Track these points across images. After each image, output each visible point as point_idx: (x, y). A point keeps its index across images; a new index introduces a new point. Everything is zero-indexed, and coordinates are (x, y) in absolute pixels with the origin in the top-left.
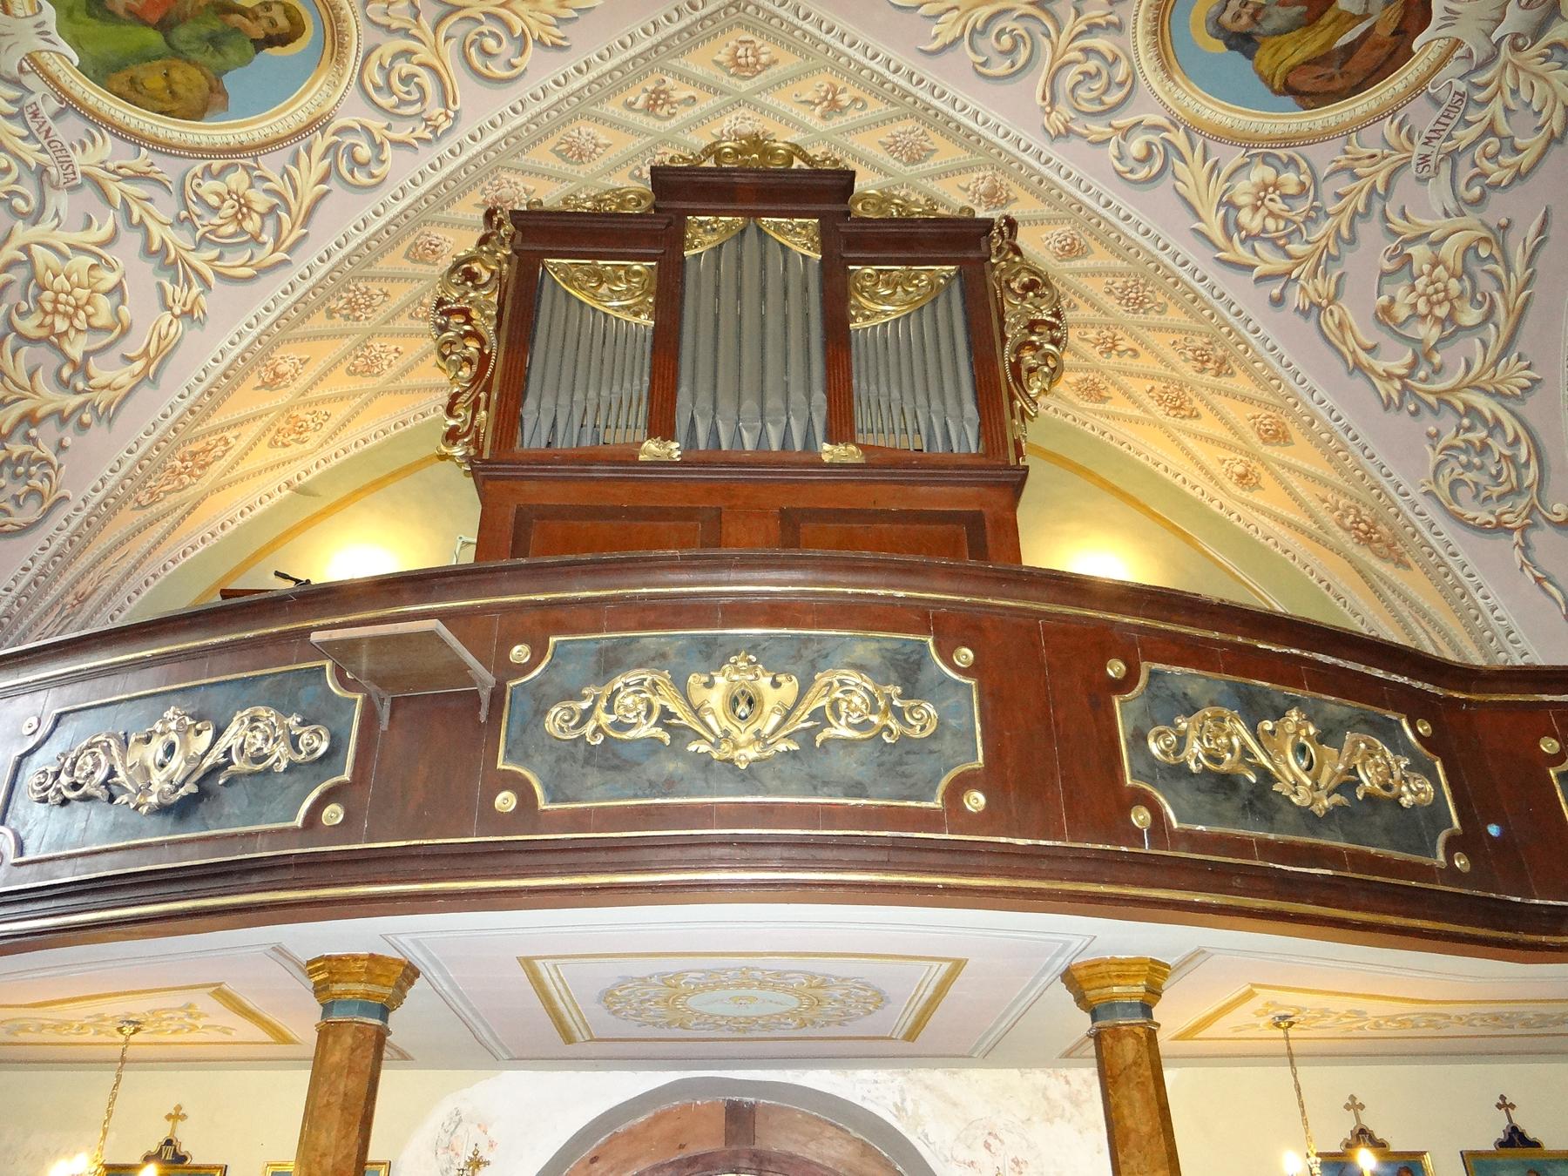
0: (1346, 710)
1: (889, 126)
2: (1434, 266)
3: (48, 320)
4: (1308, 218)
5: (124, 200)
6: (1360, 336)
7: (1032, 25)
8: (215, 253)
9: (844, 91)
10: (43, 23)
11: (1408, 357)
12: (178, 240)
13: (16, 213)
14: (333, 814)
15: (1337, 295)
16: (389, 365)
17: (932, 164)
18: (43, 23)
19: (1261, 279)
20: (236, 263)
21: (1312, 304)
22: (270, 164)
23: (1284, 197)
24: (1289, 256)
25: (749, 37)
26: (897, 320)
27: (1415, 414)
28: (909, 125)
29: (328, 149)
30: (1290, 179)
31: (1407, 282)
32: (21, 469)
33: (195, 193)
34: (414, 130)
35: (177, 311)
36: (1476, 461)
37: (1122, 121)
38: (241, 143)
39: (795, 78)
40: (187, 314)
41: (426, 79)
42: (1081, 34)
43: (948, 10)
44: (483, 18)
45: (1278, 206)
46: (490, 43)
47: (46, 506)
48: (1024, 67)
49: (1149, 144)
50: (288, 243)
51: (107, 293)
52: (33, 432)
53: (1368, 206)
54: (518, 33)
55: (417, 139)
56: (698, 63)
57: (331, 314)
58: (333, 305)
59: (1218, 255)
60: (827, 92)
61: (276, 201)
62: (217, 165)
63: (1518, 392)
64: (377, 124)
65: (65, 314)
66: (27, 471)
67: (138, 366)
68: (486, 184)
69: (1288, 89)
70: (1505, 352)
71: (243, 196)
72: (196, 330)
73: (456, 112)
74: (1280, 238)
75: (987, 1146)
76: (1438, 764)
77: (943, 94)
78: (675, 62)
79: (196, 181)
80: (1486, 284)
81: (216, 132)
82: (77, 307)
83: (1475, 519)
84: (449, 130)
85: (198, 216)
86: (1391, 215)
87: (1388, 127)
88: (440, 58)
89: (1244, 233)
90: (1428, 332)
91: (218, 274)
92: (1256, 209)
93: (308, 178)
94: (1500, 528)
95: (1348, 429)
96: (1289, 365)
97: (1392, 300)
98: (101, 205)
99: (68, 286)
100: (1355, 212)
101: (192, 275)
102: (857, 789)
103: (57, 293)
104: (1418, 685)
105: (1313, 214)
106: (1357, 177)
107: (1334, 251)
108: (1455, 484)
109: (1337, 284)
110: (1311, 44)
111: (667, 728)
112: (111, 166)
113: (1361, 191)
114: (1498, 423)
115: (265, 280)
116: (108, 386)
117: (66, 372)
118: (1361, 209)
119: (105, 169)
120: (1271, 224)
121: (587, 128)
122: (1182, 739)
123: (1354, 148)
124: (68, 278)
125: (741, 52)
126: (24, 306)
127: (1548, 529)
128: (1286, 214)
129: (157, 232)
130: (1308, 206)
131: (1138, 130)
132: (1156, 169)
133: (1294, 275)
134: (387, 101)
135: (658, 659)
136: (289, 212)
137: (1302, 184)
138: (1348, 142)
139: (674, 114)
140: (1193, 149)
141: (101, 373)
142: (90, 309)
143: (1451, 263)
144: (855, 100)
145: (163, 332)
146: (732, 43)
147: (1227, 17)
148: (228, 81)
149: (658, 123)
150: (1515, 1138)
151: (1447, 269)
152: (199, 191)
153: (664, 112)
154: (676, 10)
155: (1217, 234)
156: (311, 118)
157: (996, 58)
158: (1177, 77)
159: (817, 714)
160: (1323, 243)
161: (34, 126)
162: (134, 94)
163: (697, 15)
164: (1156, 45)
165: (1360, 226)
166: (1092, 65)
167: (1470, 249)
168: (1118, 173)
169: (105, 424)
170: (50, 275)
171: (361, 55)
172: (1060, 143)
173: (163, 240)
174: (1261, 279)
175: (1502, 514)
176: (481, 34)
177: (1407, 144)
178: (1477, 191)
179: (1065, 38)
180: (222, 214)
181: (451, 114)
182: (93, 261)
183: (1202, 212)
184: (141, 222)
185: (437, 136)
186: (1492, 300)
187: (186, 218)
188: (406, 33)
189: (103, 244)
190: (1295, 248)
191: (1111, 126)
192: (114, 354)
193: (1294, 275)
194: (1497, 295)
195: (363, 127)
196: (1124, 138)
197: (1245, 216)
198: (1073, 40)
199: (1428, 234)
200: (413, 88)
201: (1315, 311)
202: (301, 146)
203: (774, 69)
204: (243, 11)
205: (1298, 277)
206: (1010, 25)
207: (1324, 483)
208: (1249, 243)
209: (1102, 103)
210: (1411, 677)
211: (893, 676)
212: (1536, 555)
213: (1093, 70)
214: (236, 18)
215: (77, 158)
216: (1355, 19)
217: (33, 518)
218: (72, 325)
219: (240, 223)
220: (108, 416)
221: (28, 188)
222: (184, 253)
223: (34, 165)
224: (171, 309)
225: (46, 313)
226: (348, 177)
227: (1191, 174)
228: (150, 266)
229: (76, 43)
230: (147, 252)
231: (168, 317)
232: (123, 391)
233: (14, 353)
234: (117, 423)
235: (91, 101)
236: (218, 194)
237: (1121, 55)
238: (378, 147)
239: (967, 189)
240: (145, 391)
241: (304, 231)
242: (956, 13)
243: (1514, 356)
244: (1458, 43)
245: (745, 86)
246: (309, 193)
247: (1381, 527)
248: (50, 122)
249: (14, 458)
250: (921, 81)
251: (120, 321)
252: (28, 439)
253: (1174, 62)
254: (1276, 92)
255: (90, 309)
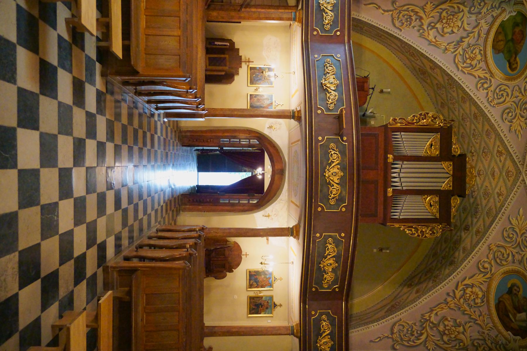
0: (339, 275)
1: (494, 208)
2: (458, 332)
3: (446, 18)
4: (469, 304)
5: (474, 32)
6: (440, 312)
7: (514, 242)
8: (461, 53)
9: (502, 197)
10: (512, 12)
11: (435, 322)
12: (465, 45)
13: (470, 8)
14: (319, 112)
15: (450, 308)
16: (440, 92)
17: (486, 218)
18: (512, 12)
19: (454, 291)
20: (459, 58)
21: (448, 302)
22: (482, 64)
23: (474, 299)
24: (460, 299)
25: (514, 174)
26: (424, 205)
27: (420, 321)
28: (495, 213)
29: (486, 77)
30: (479, 301)
31: (454, 325)
32: (409, 20)
33: (476, 48)
34: (491, 97)
35: (447, 47)
36: (409, 332)
37: (493, 262)
38: (487, 58)
39: (506, 185)
40: (446, 49)
41: (502, 99)
42: (512, 253)
43: (518, 222)
44: (516, 113)
45: (472, 298)
46: (510, 114)
47: (400, 27)
48: (505, 239)
49: (487, 268)
50: (464, 70)
51: (452, 30)
52: (418, 20)
53: (473, 319)
54: (513, 121)
55: (489, 98)
56: (508, 163)
57: (448, 80)
58: (450, 80)
59: (460, 282)
60: (502, 193)
61: (474, 66)
62: (482, 52)
63: (427, 345)
64: (492, 88)
65: (447, 21)
66: (408, 21)
67: (434, 40)
68: (479, 114)
69: (500, 302)
70: (436, 344)
71: (475, 59)
72: (442, 52)
73: (495, 107)
74: (464, 297)
75: (275, 214)
76: (330, 290)
77: (500, 220)
78: (508, 157)
79: (479, 48)
80: (454, 344)
81: (490, 52)
82: (449, 24)
83: (395, 328)
84: (491, 105)
85: (470, 49)
86: (470, 323)
87: (491, 325)
88: (507, 103)
89: (465, 289)
90: (441, 328)
91: (456, 55)
92: (472, 292)
93: (481, 73)
94: (392, 333)
95: (417, 305)
96: (432, 295)
97: (449, 321)
98: (473, 26)
99: (454, 21)
100: (471, 315)
101: (455, 49)
102: (321, 191)
103: (452, 19)
104: (345, 290)
105: (470, 305)
106: (479, 316)
107: (461, 309)
108: (404, 327)
109: (453, 309)
110: (510, 308)
111: (331, 162)
112: (482, 29)
113: (476, 317)
114: (419, 339)
115: (454, 65)
116: (429, 34)
117: (433, 24)
118: (472, 317)
119: (481, 27)
120: (468, 295)
121: (493, 136)
122: (331, 244)
123: (486, 317)
124: (456, 21)
125: (511, 173)
126: (449, 12)
127: (393, 343)
128: (470, 299)
129: (466, 40)
130: (473, 304)
131: (490, 266)
132: (482, 270)
133: (455, 299)
134: (497, 91)
135: (342, 160)
136: (472, 69)
137: (478, 303)
138: (487, 315)
139: (497, 157)
140: (486, 279)
141: (432, 33)
142: (448, 27)
143: (458, 336)
144: (500, 200)
145: (442, 44)
146: (513, 171)
147: (515, 288)
148: (501, 54)
149: (495, 153)
150: (275, 305)
151: (457, 335)
152: (476, 49)
153: (498, 155)
154: (519, 158)
155: (466, 282)
156: (493, 73)
157: (507, 233)
158: (503, 275)
159: (333, 186)
160: (463, 307)
161: (490, 11)
162: (497, 33)
163: (518, 163)
164: (510, 271)
165: (467, 317)
166: (505, 256)
167: (462, 341)
168: (480, 261)
169: (419, 35)
170: (456, 17)
171: (507, 84)
172: (487, 248)
173: (465, 41)
174: (454, 291)
175: (396, 335)
176: (512, 112)
177: (487, 329)
178: (476, 344)
179: (512, 249)
180: (471, 54)
181: (495, 105)
182: (460, 26)
183: (471, 280)
184: (468, 36)
185: (489, 102)
186: (450, 344)
187: (470, 46)
188: (512, 95)
189: (464, 28)
190: (462, 300)
191: (492, 260)
192: (437, 34)
193: (455, 299)
194: (450, 346)
195: (491, 85)
196: (489, 263)
197: (470, 289)
198: (511, 252)
199: (466, 332)
200: (500, 96)
201: (446, 303)
202: (487, 71)
203: (508, 181)
204: (515, 58)
205: (454, 300)
206: (515, 237)
207: (406, 300)
208: (463, 290)
209: (497, 258)
210: (346, 289)
211: (340, 198)
212: (386, 339)
213: (504, 256)
214: (514, 56)
215: (483, 21)
216: (515, 318)
217: (397, 25)
218: (444, 23)
219: (469, 58)
220: (421, 36)
221: (476, 10)
222: (462, 46)
223: (481, 11)
224: (448, 45)
225: (447, 17)
226: (480, 82)
227: (480, 278)
228: (458, 39)
229: (508, 20)
230: (462, 38)
231: (445, 45)
232: (428, 38)
233: (438, 12)
234: (420, 38)
235: (496, 23)
236: (476, 53)
237: (507, 263)
238: (487, 89)
239: (480, 226)
240: (427, 43)
241: (466, 73)
242: (517, 224)
243: (435, 347)
244: (510, 342)
245: (504, 174)
246: (476, 74)
247: (394, 309)
248: (491, 14)
249: (412, 18)
250: (503, 215)
251: (445, 34)
252: (416, 19)
253: (506, 275)
254: (499, 299)
255: (448, 27)
